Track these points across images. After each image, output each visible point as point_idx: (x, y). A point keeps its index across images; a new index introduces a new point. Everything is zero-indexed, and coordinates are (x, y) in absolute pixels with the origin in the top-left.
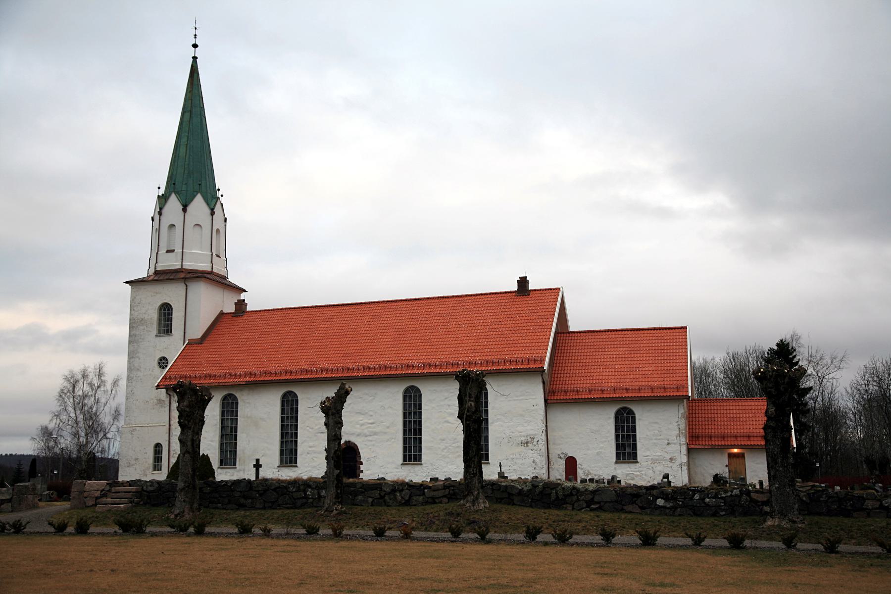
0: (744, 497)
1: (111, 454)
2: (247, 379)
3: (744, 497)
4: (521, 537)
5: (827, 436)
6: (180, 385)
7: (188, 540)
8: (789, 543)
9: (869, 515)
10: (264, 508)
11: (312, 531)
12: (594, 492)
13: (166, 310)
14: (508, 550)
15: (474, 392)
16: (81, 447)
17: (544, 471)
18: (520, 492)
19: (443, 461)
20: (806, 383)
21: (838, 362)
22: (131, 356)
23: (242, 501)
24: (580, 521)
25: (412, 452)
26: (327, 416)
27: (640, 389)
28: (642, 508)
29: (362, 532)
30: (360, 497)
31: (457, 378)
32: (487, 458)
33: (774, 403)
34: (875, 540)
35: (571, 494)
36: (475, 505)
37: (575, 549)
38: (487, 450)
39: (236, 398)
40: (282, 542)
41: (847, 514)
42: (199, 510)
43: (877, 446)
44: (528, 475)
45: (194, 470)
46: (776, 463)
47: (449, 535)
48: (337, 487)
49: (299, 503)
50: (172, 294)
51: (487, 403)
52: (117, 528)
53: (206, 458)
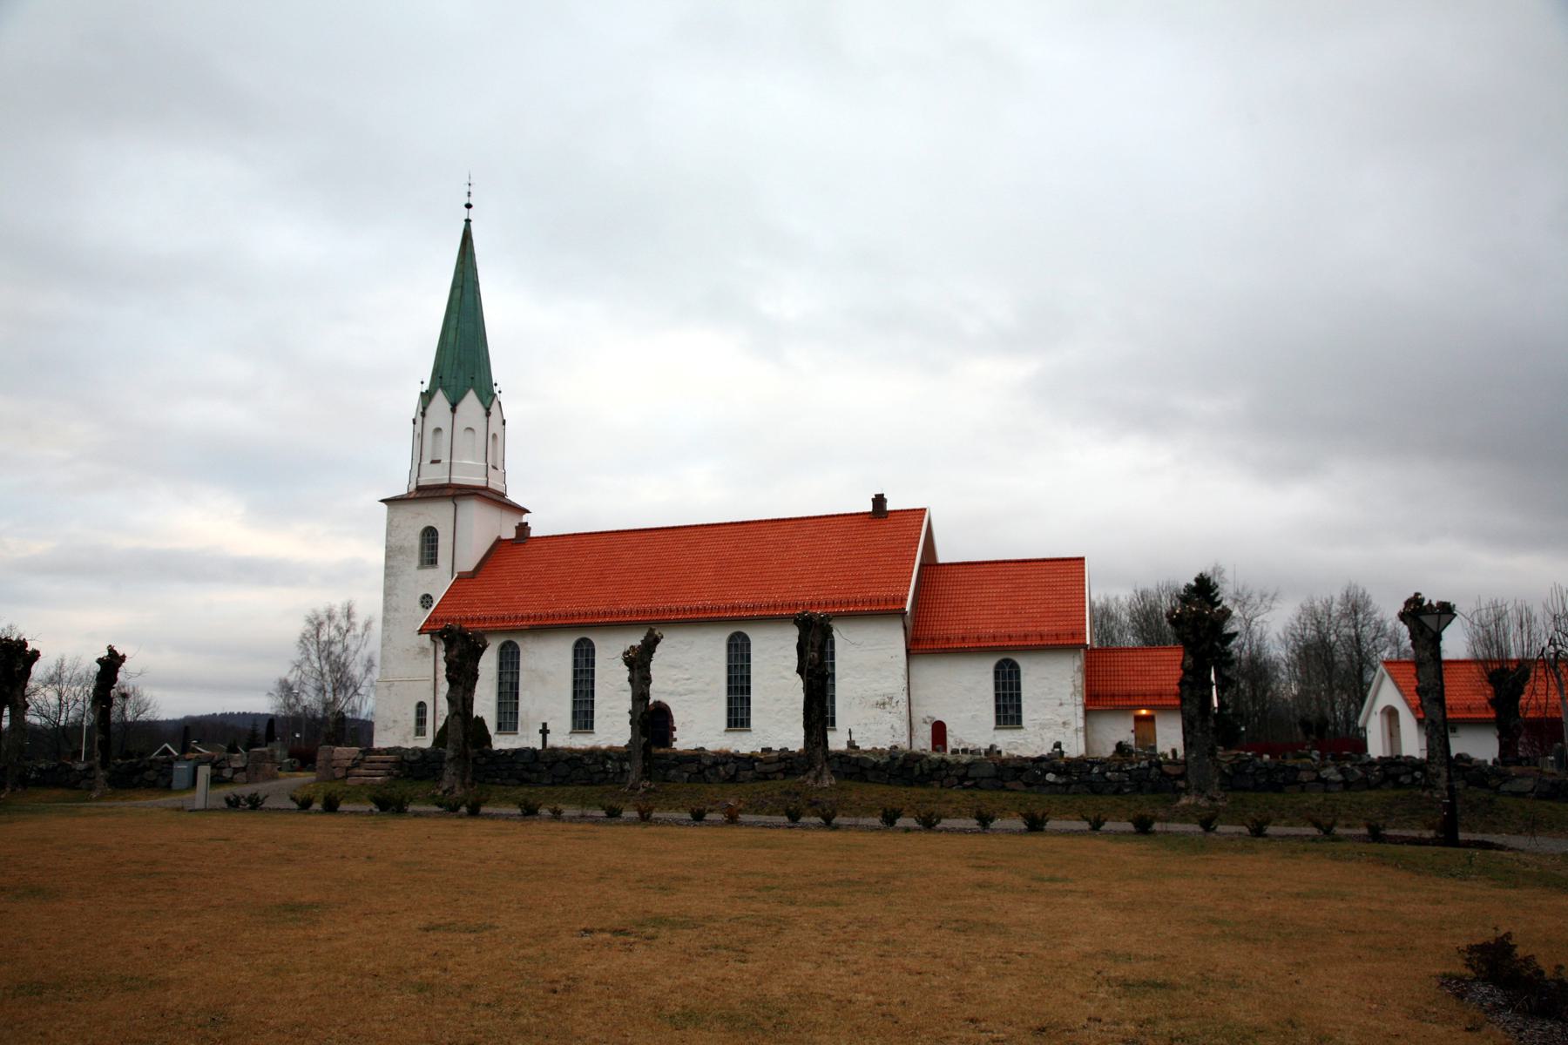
0: (1154, 770)
1: (363, 715)
2: (531, 622)
3: (1154, 770)
4: (876, 821)
5: (1254, 690)
6: (449, 630)
7: (460, 822)
8: (1207, 825)
9: (1303, 790)
10: (553, 784)
11: (613, 813)
12: (968, 766)
13: (430, 535)
14: (860, 838)
15: (818, 640)
16: (327, 705)
17: (905, 739)
18: (876, 766)
19: (778, 725)
20: (1230, 628)
21: (1270, 598)
22: (388, 592)
23: (526, 775)
24: (950, 802)
25: (738, 717)
26: (631, 669)
27: (1026, 636)
28: (1028, 785)
29: (676, 815)
30: (673, 772)
31: (796, 622)
32: (833, 723)
33: (1192, 653)
34: (1310, 819)
35: (939, 768)
36: (819, 782)
37: (943, 836)
38: (833, 713)
39: (516, 646)
40: (576, 827)
41: (1277, 788)
42: (472, 785)
43: (1314, 704)
44: (885, 744)
45: (465, 736)
46: (1193, 727)
47: (785, 819)
48: (644, 759)
49: (597, 778)
50: (438, 515)
51: (833, 654)
52: (372, 806)
53: (480, 721)
